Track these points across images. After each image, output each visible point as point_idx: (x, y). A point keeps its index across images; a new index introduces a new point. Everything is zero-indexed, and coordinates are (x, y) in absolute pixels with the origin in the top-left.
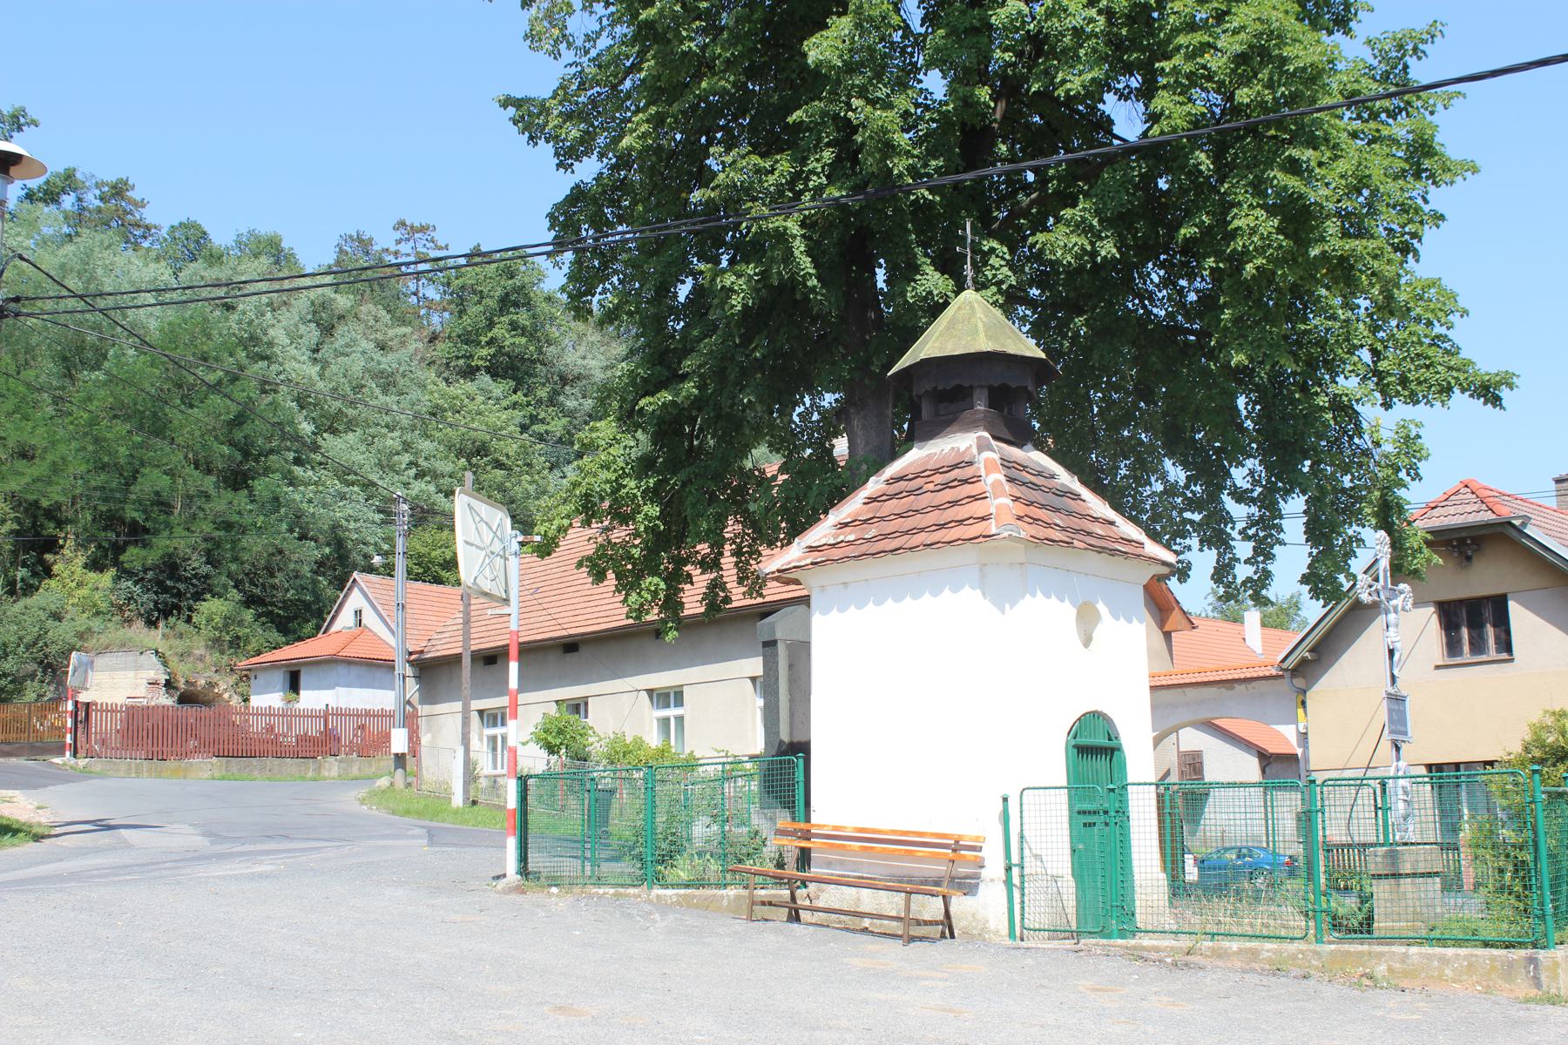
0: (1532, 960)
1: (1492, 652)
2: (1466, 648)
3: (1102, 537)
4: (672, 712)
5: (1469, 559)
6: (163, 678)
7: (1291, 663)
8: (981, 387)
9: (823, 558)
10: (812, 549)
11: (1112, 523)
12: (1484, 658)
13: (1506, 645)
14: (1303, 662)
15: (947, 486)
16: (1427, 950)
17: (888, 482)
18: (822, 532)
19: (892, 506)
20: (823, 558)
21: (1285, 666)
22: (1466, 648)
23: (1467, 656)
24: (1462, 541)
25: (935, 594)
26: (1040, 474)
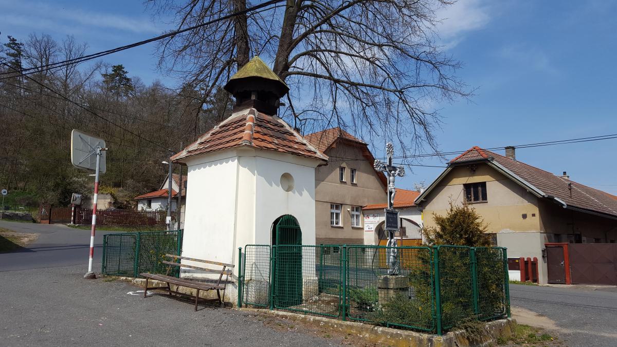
0: (430, 340)
1: (481, 200)
2: (94, 175)
3: (296, 149)
4: (335, 211)
5: (474, 171)
6: (113, 202)
7: (418, 202)
8: (254, 91)
9: (192, 156)
10: (189, 152)
11: (305, 145)
12: (478, 202)
13: (485, 197)
14: (422, 201)
15: (236, 128)
16: (387, 329)
17: (220, 127)
18: (194, 146)
19: (219, 136)
20: (192, 156)
21: (416, 203)
22: (94, 175)
23: (481, 200)
24: (472, 165)
25: (204, 168)
26: (276, 125)
